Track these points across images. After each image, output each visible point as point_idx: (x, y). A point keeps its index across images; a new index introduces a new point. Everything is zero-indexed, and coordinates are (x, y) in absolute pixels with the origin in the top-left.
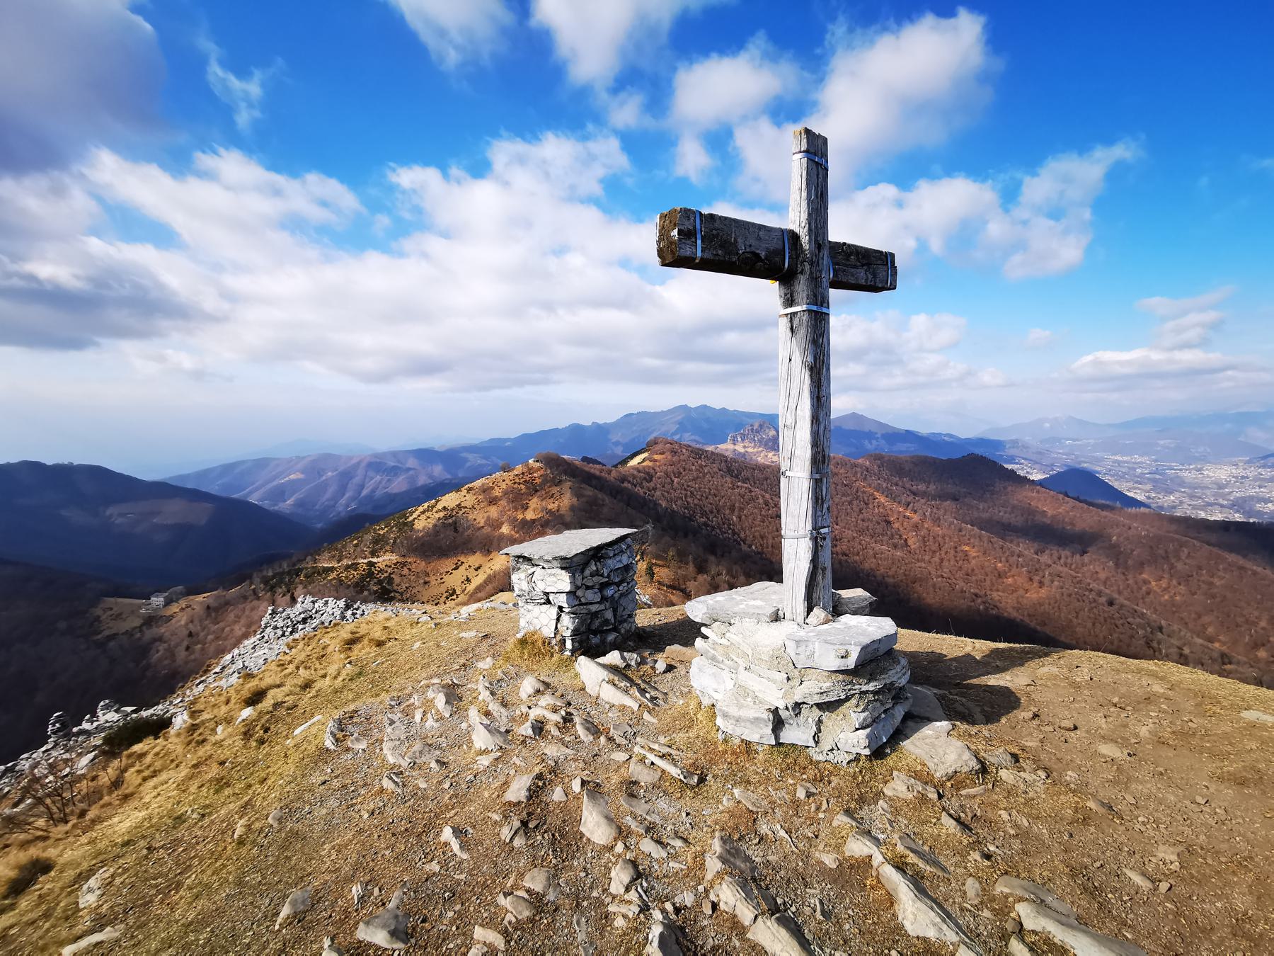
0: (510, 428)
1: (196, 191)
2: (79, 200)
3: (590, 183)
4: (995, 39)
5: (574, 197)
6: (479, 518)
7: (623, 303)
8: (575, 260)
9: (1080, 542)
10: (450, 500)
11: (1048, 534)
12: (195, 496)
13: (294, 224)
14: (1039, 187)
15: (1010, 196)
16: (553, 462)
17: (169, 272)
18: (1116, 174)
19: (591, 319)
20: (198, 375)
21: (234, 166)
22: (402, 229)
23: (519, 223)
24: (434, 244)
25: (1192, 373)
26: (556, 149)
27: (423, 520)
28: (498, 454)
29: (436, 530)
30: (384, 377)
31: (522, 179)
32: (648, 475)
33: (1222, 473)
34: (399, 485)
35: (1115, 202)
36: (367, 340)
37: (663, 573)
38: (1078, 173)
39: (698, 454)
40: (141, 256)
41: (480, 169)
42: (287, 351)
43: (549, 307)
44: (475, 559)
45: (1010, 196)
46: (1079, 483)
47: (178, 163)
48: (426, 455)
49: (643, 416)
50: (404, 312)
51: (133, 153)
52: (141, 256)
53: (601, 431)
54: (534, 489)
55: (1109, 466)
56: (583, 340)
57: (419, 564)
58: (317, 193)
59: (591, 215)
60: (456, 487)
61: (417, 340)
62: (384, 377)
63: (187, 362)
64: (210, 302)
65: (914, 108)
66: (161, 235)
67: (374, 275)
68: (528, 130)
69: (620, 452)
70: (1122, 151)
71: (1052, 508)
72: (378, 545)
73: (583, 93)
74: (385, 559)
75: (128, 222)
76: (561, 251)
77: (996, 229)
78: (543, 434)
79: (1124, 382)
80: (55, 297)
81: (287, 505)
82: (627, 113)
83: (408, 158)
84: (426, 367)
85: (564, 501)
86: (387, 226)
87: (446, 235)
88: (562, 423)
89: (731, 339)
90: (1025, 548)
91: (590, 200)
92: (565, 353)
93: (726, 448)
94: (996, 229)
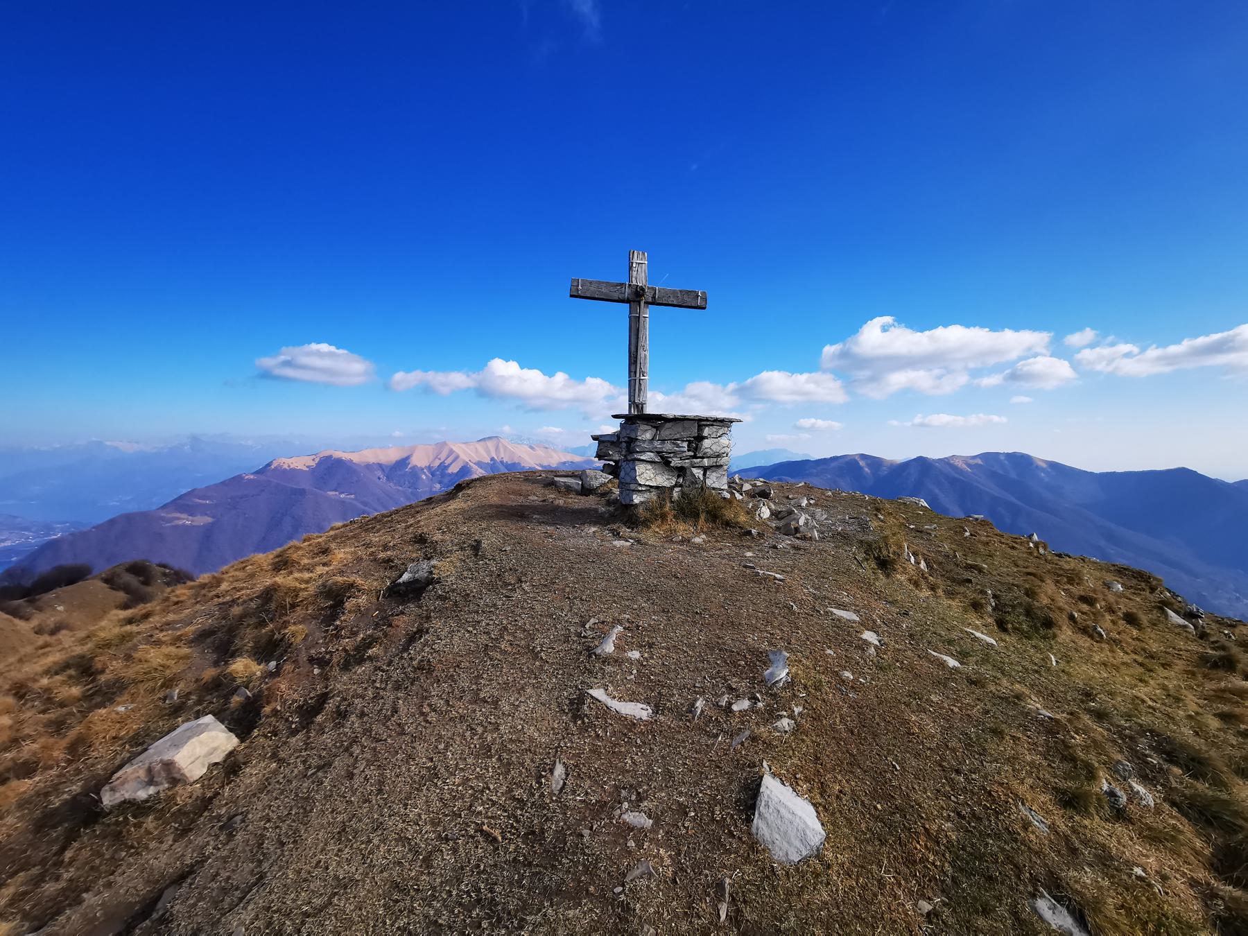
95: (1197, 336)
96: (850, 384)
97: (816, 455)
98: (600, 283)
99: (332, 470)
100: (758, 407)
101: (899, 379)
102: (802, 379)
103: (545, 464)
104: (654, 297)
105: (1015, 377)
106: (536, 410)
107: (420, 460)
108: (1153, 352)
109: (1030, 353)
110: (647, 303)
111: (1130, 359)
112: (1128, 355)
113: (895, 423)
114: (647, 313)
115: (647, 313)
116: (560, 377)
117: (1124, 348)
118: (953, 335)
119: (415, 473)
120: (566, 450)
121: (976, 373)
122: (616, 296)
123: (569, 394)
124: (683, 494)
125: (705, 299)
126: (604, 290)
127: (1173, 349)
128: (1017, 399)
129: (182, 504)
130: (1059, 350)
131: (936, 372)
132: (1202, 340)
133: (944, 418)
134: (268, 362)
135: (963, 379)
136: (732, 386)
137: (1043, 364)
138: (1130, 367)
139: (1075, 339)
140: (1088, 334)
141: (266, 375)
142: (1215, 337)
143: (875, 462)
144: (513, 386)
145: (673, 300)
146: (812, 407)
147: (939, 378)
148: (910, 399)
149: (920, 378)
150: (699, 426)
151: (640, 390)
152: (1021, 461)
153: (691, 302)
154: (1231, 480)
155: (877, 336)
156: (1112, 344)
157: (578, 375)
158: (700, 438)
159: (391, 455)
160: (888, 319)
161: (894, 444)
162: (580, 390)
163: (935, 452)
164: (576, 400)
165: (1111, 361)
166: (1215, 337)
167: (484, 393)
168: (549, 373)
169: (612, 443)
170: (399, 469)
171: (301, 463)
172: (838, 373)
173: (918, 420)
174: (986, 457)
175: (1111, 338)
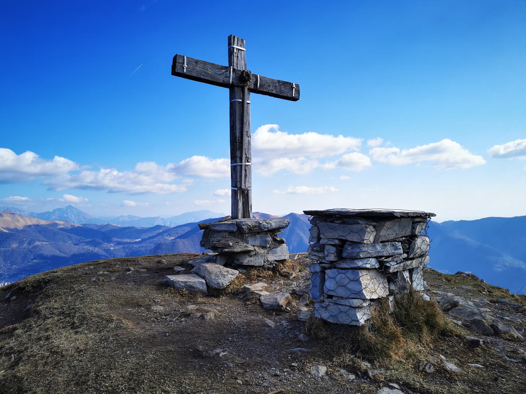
95: (422, 145)
98: (205, 63)
100: (189, 181)
103: (12, 227)
104: (256, 84)
105: (341, 164)
106: (115, 192)
108: (404, 152)
109: (350, 151)
110: (251, 90)
111: (396, 156)
112: (394, 153)
113: (277, 191)
114: (254, 101)
115: (254, 101)
116: (29, 156)
117: (395, 149)
118: (311, 138)
120: (32, 215)
121: (323, 161)
122: (221, 79)
123: (37, 169)
124: (397, 303)
125: (298, 92)
126: (210, 72)
127: (412, 150)
128: (343, 177)
130: (365, 150)
131: (302, 158)
132: (425, 147)
133: (304, 189)
135: (316, 164)
136: (171, 166)
137: (357, 157)
138: (394, 160)
139: (371, 143)
140: (379, 140)
142: (432, 145)
145: (271, 89)
147: (303, 163)
148: (286, 176)
150: (413, 223)
151: (246, 176)
153: (286, 92)
154: (440, 222)
156: (390, 146)
158: (413, 237)
160: (275, 126)
162: (48, 166)
164: (44, 174)
165: (387, 156)
166: (432, 145)
168: (18, 151)
169: (231, 233)
173: (290, 190)
175: (389, 143)
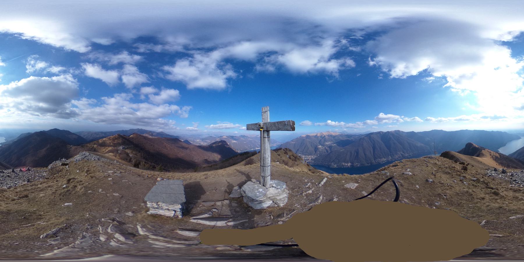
0: (114, 130)
1: (81, 102)
2: (71, 105)
3: (128, 98)
4: (180, 93)
5: (125, 100)
6: (108, 142)
7: (131, 114)
8: (125, 108)
9: (186, 148)
10: (104, 139)
11: (183, 148)
12: (76, 135)
13: (89, 104)
14: (184, 108)
15: (181, 109)
16: (119, 135)
17: (76, 110)
18: (191, 109)
19: (126, 115)
20: (78, 121)
21: (84, 99)
22: (102, 104)
23: (117, 103)
24: (105, 106)
25: (196, 130)
26: (123, 95)
27: (100, 141)
28: (112, 133)
29: (102, 143)
30: (98, 122)
31: (118, 98)
32: (133, 138)
33: (198, 141)
34: (98, 136)
35: (190, 112)
36: (96, 117)
37: (134, 152)
38: (187, 108)
39: (140, 135)
40: (75, 109)
41: (112, 97)
42: (87, 118)
43: (121, 114)
44: (107, 148)
45: (181, 109)
46: (187, 142)
47: (79, 100)
48: (102, 133)
49: (133, 129)
50: (101, 114)
51: (75, 100)
52: (75, 109)
53: (126, 131)
54: (116, 139)
55: (189, 139)
56: (125, 118)
57: (99, 147)
58: (93, 101)
59: (128, 102)
60: (105, 137)
61: (102, 117)
62: (98, 122)
63: (77, 120)
64: (80, 114)
65: (171, 97)
66: (77, 107)
67: (98, 110)
68: (120, 93)
69: (129, 134)
70: (191, 107)
71: (184, 145)
72: (95, 144)
73: (129, 89)
74: (95, 146)
75: (74, 106)
76: (123, 106)
77: (180, 112)
78: (118, 131)
79: (191, 131)
80: (67, 114)
81: (85, 137)
82: (134, 91)
83: (103, 96)
84: (103, 121)
85: (120, 141)
86: (101, 104)
87: (107, 104)
88: (121, 130)
89: (146, 120)
90: (181, 149)
91: (128, 101)
92: (122, 120)
93: (144, 135)
94: (180, 112)
96: (379, 122)
97: (375, 131)
99: (308, 137)
101: (384, 121)
102: (372, 121)
107: (318, 135)
118: (390, 116)
119: (318, 137)
129: (292, 141)
134: (301, 123)
141: (300, 125)
143: (382, 132)
144: (330, 124)
146: (374, 125)
148: (386, 124)
149: (387, 121)
152: (399, 131)
155: (382, 115)
157: (339, 122)
159: (315, 134)
161: (385, 130)
162: (340, 124)
163: (390, 130)
167: (327, 125)
170: (316, 136)
171: (304, 136)
172: (377, 120)
174: (395, 131)
